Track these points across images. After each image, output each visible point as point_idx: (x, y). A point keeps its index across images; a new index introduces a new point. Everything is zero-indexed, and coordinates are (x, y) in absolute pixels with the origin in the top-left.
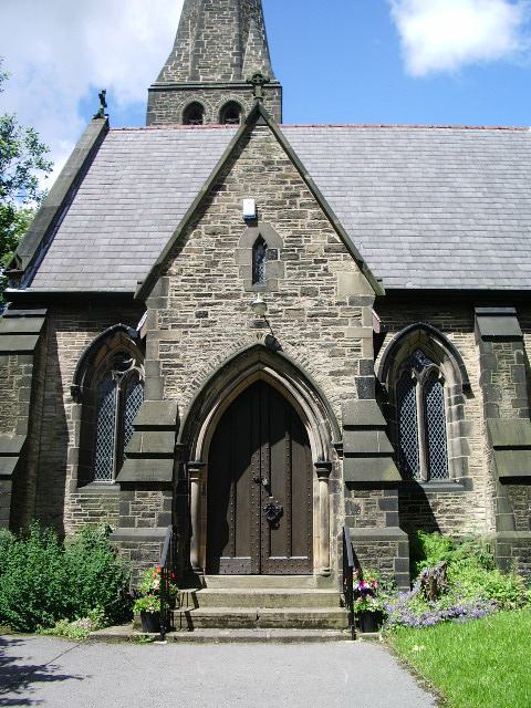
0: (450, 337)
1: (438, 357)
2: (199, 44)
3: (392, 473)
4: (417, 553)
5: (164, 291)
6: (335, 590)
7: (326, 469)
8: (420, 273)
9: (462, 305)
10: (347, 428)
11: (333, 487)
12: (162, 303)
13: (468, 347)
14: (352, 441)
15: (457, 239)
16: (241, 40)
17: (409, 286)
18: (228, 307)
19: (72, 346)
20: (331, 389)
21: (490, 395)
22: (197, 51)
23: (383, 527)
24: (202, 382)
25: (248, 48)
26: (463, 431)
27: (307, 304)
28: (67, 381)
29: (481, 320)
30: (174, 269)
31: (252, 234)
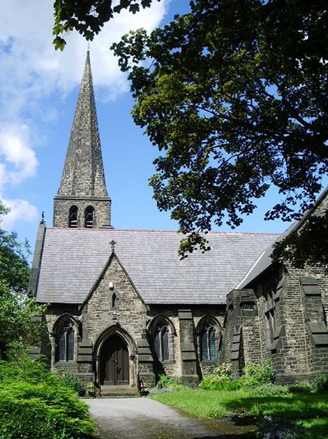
0: (170, 318)
1: (167, 324)
2: (75, 177)
3: (151, 359)
4: (158, 379)
5: (87, 309)
6: (136, 387)
7: (133, 358)
8: (162, 298)
9: (175, 309)
10: (139, 347)
11: (135, 363)
12: (86, 312)
13: (176, 322)
14: (140, 350)
15: (175, 284)
16: (93, 176)
17: (158, 302)
18: (106, 314)
19: (52, 319)
20: (135, 337)
21: (182, 336)
22: (74, 180)
23: (148, 372)
24: (99, 335)
25: (96, 180)
26: (174, 346)
27: (128, 313)
28: (50, 330)
29: (180, 314)
30: (89, 303)
31: (112, 292)
